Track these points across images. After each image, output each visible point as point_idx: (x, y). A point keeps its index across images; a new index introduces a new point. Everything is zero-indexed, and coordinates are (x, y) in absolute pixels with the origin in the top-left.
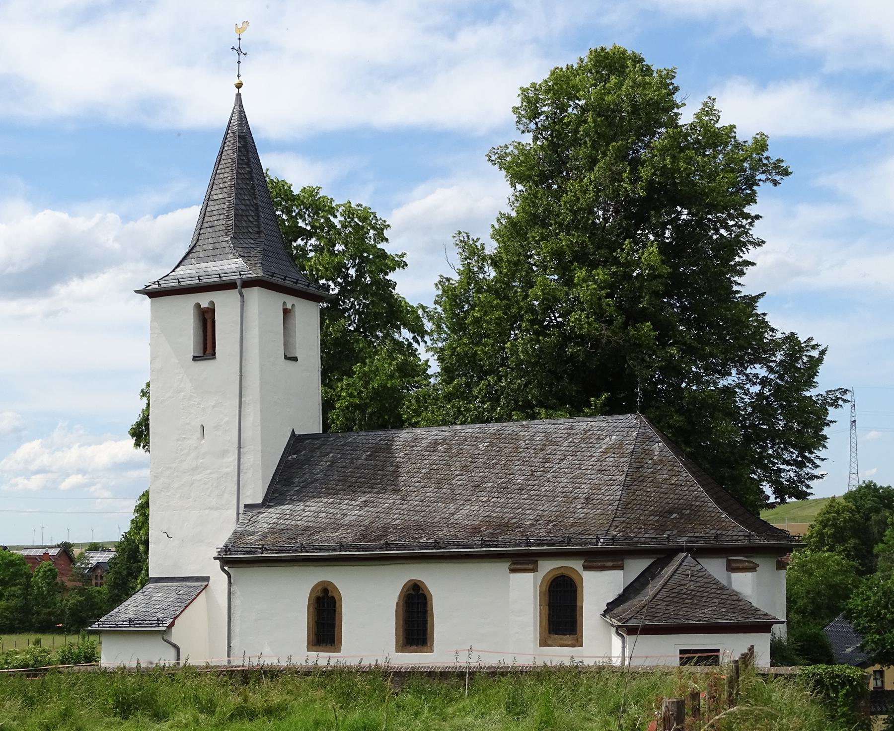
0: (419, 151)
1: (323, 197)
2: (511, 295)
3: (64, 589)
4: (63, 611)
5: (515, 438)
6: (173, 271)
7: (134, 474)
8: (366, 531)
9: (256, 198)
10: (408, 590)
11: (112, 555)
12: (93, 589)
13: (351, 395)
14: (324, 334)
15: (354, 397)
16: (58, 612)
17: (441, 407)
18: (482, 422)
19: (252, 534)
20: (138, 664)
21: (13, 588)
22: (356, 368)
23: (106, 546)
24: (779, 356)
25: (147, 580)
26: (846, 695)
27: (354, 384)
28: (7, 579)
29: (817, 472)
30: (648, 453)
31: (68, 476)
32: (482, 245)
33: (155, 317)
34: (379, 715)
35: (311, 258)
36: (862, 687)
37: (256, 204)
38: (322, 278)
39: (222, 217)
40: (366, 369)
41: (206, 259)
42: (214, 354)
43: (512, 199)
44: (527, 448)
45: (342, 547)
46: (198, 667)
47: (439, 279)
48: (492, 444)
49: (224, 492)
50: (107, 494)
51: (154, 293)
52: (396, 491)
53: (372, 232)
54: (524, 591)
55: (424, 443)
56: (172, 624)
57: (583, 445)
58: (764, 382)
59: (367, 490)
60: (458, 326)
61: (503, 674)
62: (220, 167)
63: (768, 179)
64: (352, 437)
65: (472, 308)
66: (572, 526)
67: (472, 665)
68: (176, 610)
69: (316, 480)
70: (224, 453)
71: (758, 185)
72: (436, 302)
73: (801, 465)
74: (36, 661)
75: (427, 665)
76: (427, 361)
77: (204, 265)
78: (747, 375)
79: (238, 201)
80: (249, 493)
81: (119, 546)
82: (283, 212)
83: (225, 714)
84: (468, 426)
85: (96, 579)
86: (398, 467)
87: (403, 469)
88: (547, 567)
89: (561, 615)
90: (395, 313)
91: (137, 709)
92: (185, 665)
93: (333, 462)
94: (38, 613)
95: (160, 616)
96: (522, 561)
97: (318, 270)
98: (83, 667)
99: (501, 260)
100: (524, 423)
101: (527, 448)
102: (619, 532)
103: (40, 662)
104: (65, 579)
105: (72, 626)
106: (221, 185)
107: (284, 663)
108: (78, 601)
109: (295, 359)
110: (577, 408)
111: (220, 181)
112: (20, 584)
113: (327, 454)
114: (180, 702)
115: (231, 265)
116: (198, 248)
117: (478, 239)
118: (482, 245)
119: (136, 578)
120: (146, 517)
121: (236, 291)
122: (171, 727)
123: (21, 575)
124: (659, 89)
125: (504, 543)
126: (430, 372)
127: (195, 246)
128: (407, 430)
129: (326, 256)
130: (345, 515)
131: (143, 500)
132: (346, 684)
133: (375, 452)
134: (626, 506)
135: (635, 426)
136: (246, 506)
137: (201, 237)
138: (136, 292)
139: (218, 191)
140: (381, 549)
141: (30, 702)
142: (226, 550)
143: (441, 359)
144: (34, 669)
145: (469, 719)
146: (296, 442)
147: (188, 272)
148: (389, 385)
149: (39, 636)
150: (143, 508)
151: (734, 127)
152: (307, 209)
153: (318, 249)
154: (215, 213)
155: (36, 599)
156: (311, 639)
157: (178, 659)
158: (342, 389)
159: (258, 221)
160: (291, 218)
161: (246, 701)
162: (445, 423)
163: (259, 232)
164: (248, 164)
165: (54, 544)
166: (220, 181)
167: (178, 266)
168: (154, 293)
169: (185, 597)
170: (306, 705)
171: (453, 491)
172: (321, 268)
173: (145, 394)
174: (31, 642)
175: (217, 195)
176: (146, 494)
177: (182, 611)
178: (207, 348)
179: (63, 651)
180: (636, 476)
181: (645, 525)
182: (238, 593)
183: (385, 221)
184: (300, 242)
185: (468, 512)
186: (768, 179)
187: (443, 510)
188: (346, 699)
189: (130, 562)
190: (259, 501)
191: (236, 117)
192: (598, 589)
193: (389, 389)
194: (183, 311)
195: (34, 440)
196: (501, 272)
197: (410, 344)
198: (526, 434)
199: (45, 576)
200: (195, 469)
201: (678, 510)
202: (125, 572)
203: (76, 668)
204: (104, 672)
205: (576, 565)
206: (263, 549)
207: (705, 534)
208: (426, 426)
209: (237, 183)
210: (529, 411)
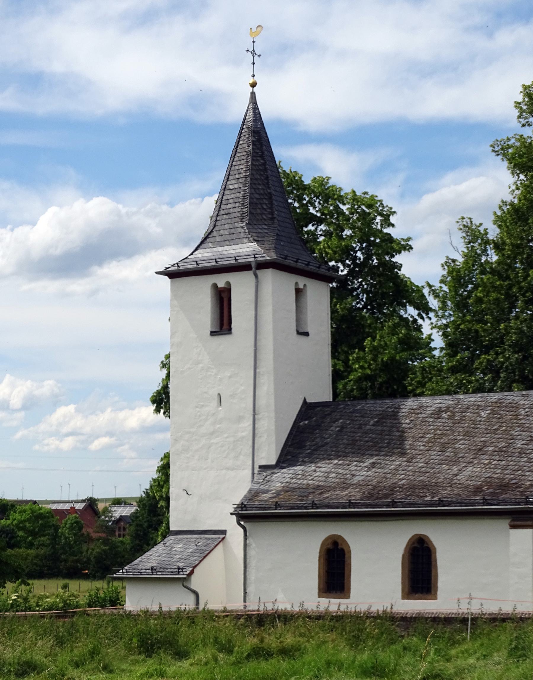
0: (430, 146)
1: (333, 186)
2: (512, 276)
3: (89, 539)
4: (89, 559)
5: (515, 407)
6: (192, 254)
7: (160, 436)
8: (374, 490)
9: (269, 188)
10: (413, 543)
11: (133, 509)
12: (116, 539)
13: (362, 367)
14: (333, 311)
15: (365, 369)
16: (85, 559)
17: (445, 378)
18: (483, 392)
19: (266, 492)
20: (161, 608)
21: (42, 538)
23: (129, 501)
25: (168, 533)
27: (364, 358)
28: (37, 530)
31: (97, 437)
32: (485, 230)
34: (386, 656)
35: (320, 242)
38: (331, 261)
39: (237, 205)
40: (375, 343)
43: (514, 187)
44: (527, 416)
45: (351, 504)
46: (216, 611)
48: (493, 412)
49: (240, 453)
50: (133, 454)
51: (173, 274)
52: (403, 454)
53: (379, 218)
55: (429, 411)
56: (192, 572)
59: (375, 453)
60: (461, 305)
61: (504, 620)
62: (236, 159)
64: (361, 405)
65: (476, 287)
67: (474, 611)
68: (195, 560)
70: (240, 419)
72: (442, 282)
74: (65, 602)
75: (432, 611)
76: (431, 335)
77: (220, 249)
80: (263, 455)
81: (140, 501)
82: (294, 200)
83: (242, 653)
84: (471, 395)
85: (119, 530)
86: (403, 432)
87: (409, 434)
90: (405, 292)
91: (159, 648)
92: (204, 609)
93: (342, 428)
94: (66, 561)
95: (181, 565)
97: (327, 254)
98: (109, 610)
99: (504, 243)
100: (524, 392)
101: (527, 416)
103: (69, 605)
104: (90, 530)
105: (97, 572)
106: (237, 176)
107: (297, 609)
108: (104, 550)
109: (307, 334)
112: (48, 534)
113: (337, 420)
114: (200, 642)
115: (247, 249)
116: (215, 233)
117: (481, 224)
118: (485, 230)
119: (157, 530)
120: (167, 476)
122: (191, 665)
123: (50, 527)
125: (505, 502)
126: (433, 345)
127: (212, 231)
128: (412, 399)
129: (335, 240)
130: (353, 475)
131: (165, 461)
132: (356, 627)
133: (382, 418)
136: (261, 467)
137: (218, 223)
139: (234, 182)
140: (388, 506)
141: (60, 641)
142: (242, 506)
143: (445, 335)
144: (65, 610)
145: (471, 661)
146: (308, 409)
147: (205, 255)
148: (398, 358)
149: (66, 581)
150: (165, 469)
152: (318, 198)
153: (327, 234)
154: (231, 201)
155: (63, 548)
156: (322, 587)
157: (197, 603)
159: (271, 208)
160: (302, 206)
161: (262, 641)
162: (448, 392)
163: (272, 219)
164: (262, 157)
165: (80, 498)
166: (236, 172)
167: (196, 249)
168: (173, 274)
169: (204, 548)
170: (318, 646)
171: (456, 454)
172: (330, 251)
173: (165, 365)
174: (59, 587)
175: (233, 185)
176: (167, 456)
177: (201, 561)
178: (223, 324)
179: (90, 596)
182: (254, 545)
183: (391, 208)
184: (311, 227)
185: (471, 474)
187: (447, 471)
188: (356, 642)
189: (152, 515)
190: (273, 462)
191: (250, 113)
193: (397, 361)
194: (202, 290)
195: (70, 404)
196: (503, 255)
197: (415, 321)
198: (526, 402)
199: (71, 528)
200: (212, 433)
202: (146, 525)
203: (102, 611)
204: (129, 615)
206: (277, 505)
208: (431, 395)
209: (252, 174)
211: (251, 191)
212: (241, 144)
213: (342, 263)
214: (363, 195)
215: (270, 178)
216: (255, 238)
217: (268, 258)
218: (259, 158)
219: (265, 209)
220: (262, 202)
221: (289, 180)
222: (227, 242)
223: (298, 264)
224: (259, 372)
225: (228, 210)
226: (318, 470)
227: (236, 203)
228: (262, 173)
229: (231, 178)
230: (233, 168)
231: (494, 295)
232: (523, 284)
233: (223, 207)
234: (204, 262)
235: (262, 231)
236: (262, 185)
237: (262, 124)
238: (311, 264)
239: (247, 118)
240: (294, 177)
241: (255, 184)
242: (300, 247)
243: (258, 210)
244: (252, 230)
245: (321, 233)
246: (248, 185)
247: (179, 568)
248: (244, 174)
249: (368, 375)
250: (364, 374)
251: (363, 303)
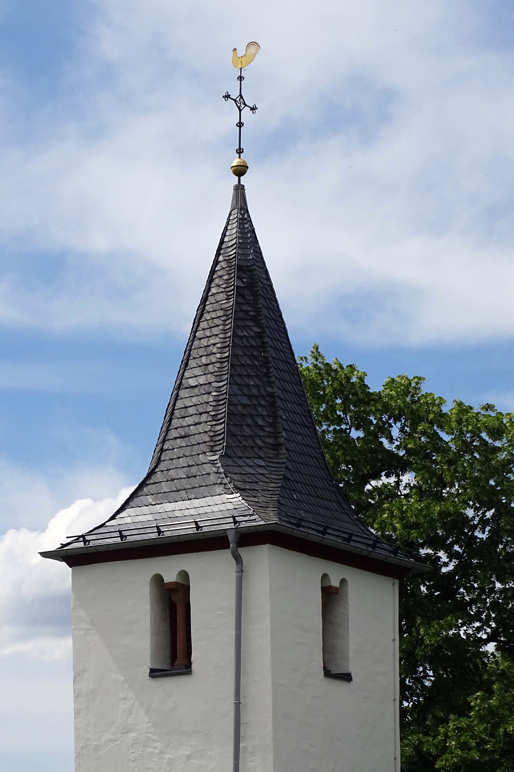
1: (426, 396)
9: (270, 384)
15: (470, 749)
22: (475, 700)
27: (470, 728)
37: (272, 395)
62: (203, 325)
79: (236, 388)
106: (204, 360)
109: (347, 677)
111: (202, 352)
115: (220, 506)
116: (158, 476)
138: (45, 555)
139: (197, 371)
147: (140, 518)
154: (191, 411)
158: (447, 737)
159: (273, 425)
163: (276, 447)
166: (202, 352)
168: (78, 556)
175: (196, 377)
178: (175, 656)
191: (233, 231)
194: (133, 587)
209: (234, 355)
211: (231, 388)
212: (213, 295)
213: (446, 552)
214: (483, 412)
215: (273, 363)
216: (238, 484)
217: (263, 523)
218: (249, 323)
219: (261, 427)
220: (254, 412)
221: (335, 385)
222: (183, 494)
223: (327, 536)
224: (245, 748)
225: (186, 429)
227: (201, 414)
228: (255, 353)
229: (192, 363)
230: (196, 343)
233: (175, 423)
234: (136, 532)
235: (253, 472)
236: (254, 379)
237: (258, 252)
238: (354, 538)
239: (226, 239)
240: (348, 379)
241: (240, 375)
242: (336, 506)
243: (247, 429)
244: (231, 469)
245: (407, 491)
246: (225, 377)
248: (218, 356)
249: (474, 761)
250: (466, 759)
251: (489, 630)
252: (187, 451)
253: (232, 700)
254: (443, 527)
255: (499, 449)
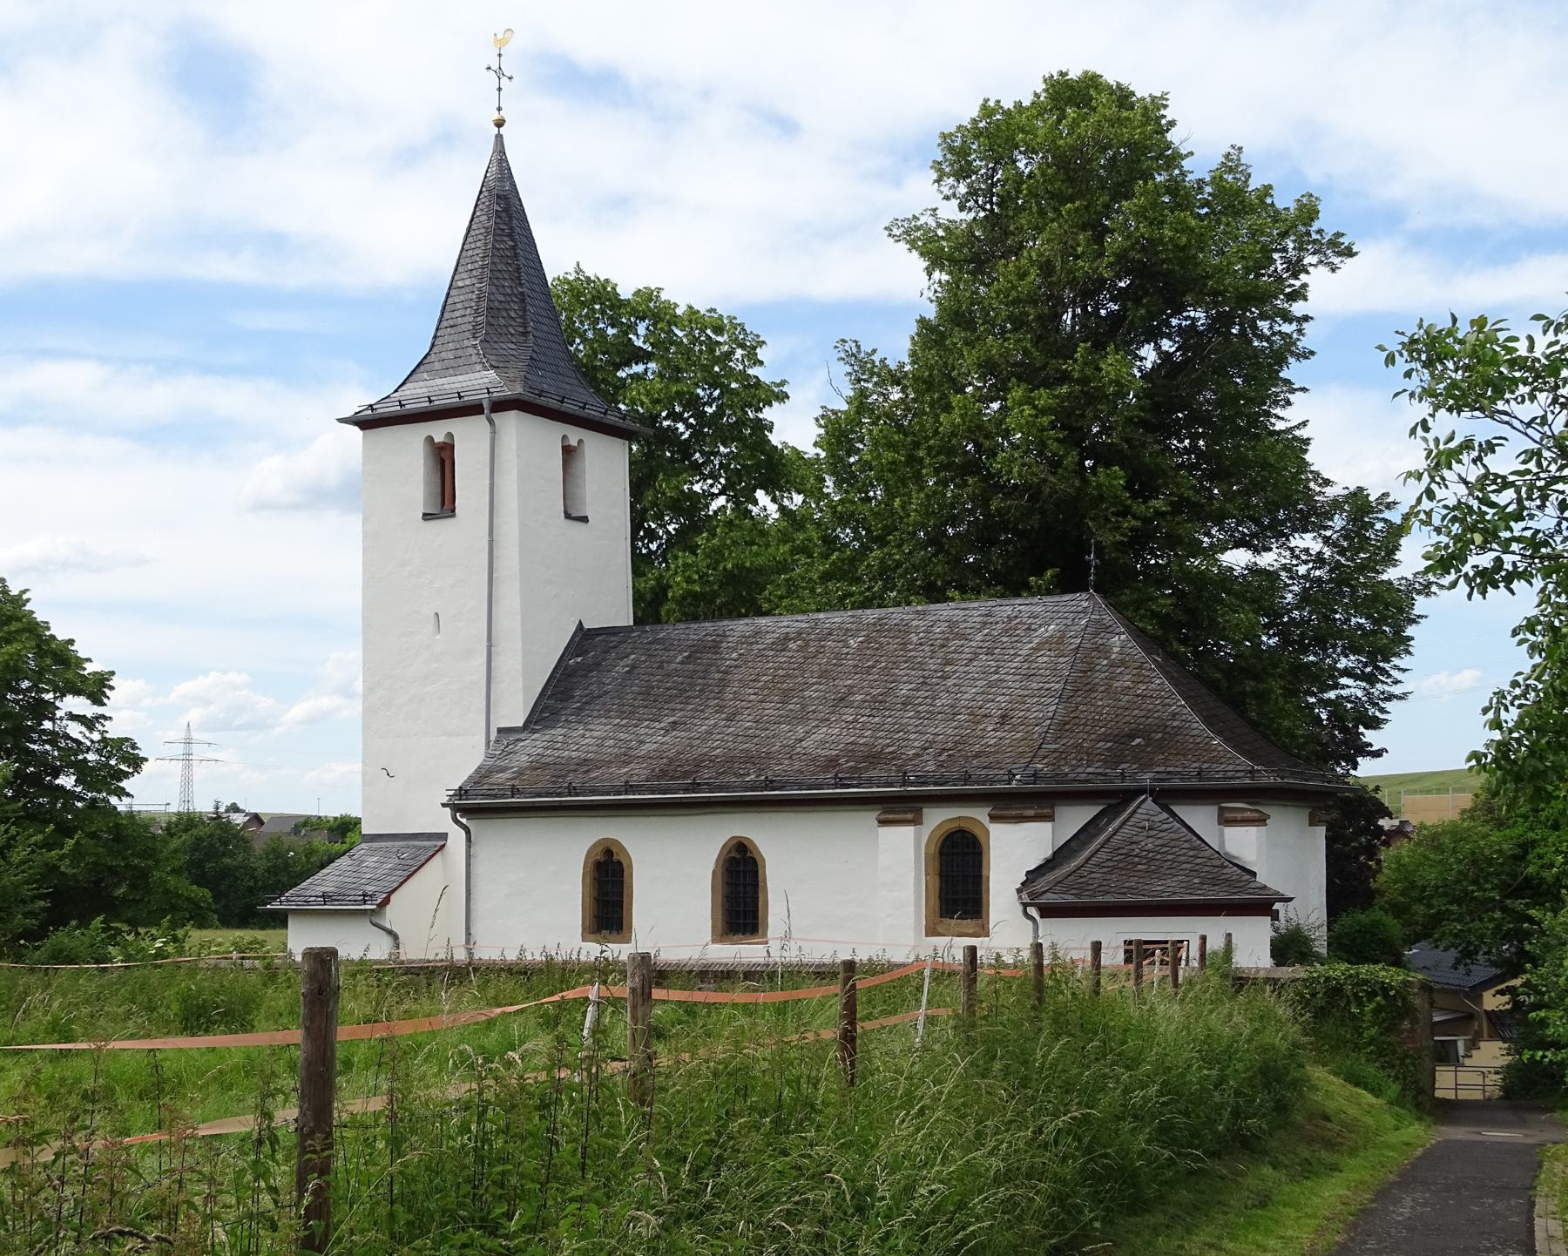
5: (904, 630)
9: (521, 285)
19: (503, 770)
24: (1338, 522)
26: (1376, 1011)
29: (1396, 690)
30: (1103, 650)
33: (367, 458)
36: (1404, 999)
41: (436, 374)
42: (453, 510)
45: (629, 788)
47: (820, 412)
48: (868, 640)
51: (368, 422)
53: (739, 353)
54: (897, 857)
56: (386, 901)
57: (1004, 639)
58: (1319, 560)
63: (1321, 262)
66: (976, 756)
69: (606, 693)
71: (1307, 272)
73: (1371, 680)
77: (439, 381)
78: (1292, 550)
88: (937, 818)
89: (957, 886)
93: (633, 667)
95: (370, 889)
96: (898, 807)
102: (1048, 765)
109: (584, 519)
110: (1013, 586)
115: (479, 380)
116: (432, 358)
117: (874, 351)
121: (483, 417)
124: (1144, 125)
134: (1063, 727)
135: (1085, 611)
136: (500, 730)
138: (341, 420)
139: (464, 275)
140: (686, 791)
142: (461, 792)
146: (584, 639)
151: (1270, 187)
163: (525, 334)
168: (368, 422)
171: (804, 706)
178: (443, 503)
180: (1081, 685)
181: (1088, 754)
185: (823, 738)
186: (1321, 262)
190: (520, 724)
192: (1014, 850)
194: (411, 444)
198: (921, 623)
201: (1144, 733)
205: (980, 814)
207: (1182, 770)
210: (934, 593)
226: (588, 734)
231: (889, 456)
232: (932, 442)
233: (446, 315)
237: (514, 185)
247: (364, 895)
252: (455, 337)
253: (487, 538)
254: (680, 404)
255: (718, 343)
